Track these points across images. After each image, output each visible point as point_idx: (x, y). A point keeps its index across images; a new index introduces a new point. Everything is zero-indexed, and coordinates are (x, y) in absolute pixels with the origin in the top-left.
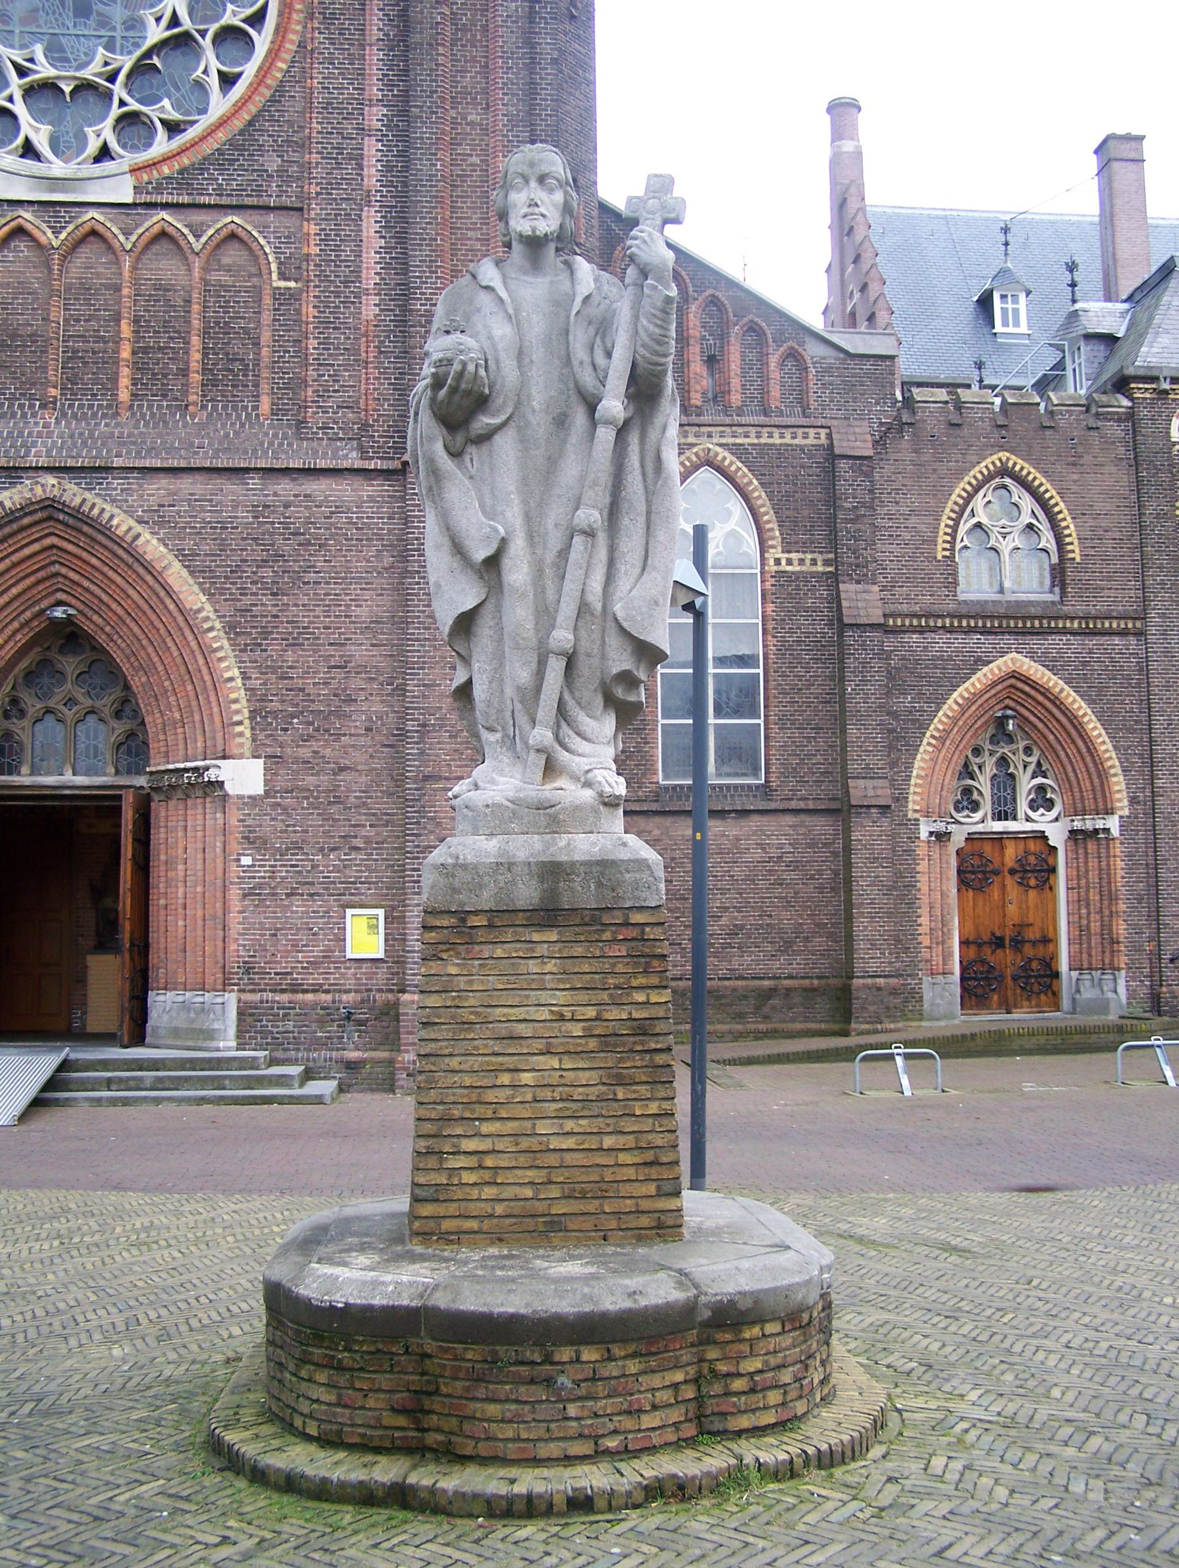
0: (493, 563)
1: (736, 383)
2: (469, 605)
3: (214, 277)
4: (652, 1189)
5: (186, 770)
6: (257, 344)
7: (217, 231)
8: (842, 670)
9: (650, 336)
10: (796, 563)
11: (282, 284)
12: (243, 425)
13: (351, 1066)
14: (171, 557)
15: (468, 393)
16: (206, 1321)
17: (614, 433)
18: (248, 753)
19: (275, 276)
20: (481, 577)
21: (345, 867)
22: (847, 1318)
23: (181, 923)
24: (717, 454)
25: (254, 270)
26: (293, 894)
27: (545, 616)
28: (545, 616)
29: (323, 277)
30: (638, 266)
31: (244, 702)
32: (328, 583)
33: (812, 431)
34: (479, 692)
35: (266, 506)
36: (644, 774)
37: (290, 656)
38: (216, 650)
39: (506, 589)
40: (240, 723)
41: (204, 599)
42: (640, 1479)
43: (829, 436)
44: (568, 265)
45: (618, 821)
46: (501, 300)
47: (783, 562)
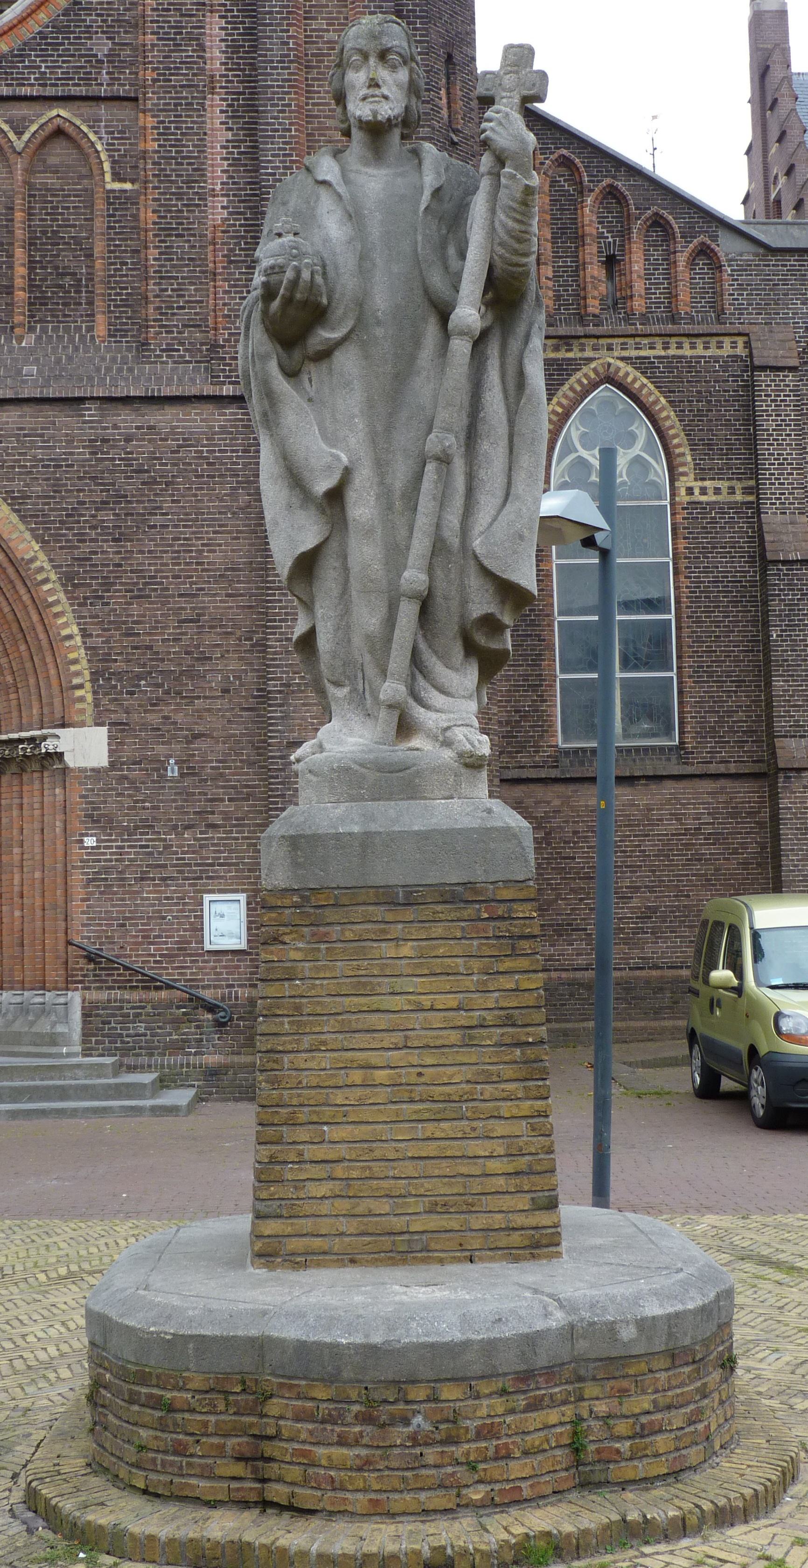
0: (336, 497)
1: (639, 287)
2: (309, 542)
3: (39, 180)
5: (21, 741)
6: (90, 256)
7: (41, 127)
8: (766, 613)
9: (509, 232)
10: (711, 492)
11: (117, 186)
12: (76, 349)
13: (213, 1073)
15: (305, 303)
17: (469, 346)
18: (89, 720)
19: (108, 177)
20: (323, 512)
21: (201, 846)
23: (17, 913)
25: (84, 171)
26: (142, 879)
27: (396, 556)
29: (162, 177)
31: (84, 663)
32: (176, 526)
33: (727, 341)
34: (324, 642)
35: (105, 441)
37: (135, 609)
38: (52, 605)
39: (351, 526)
40: (81, 686)
41: (37, 547)
43: (748, 345)
44: (416, 153)
45: (482, 788)
47: (697, 491)
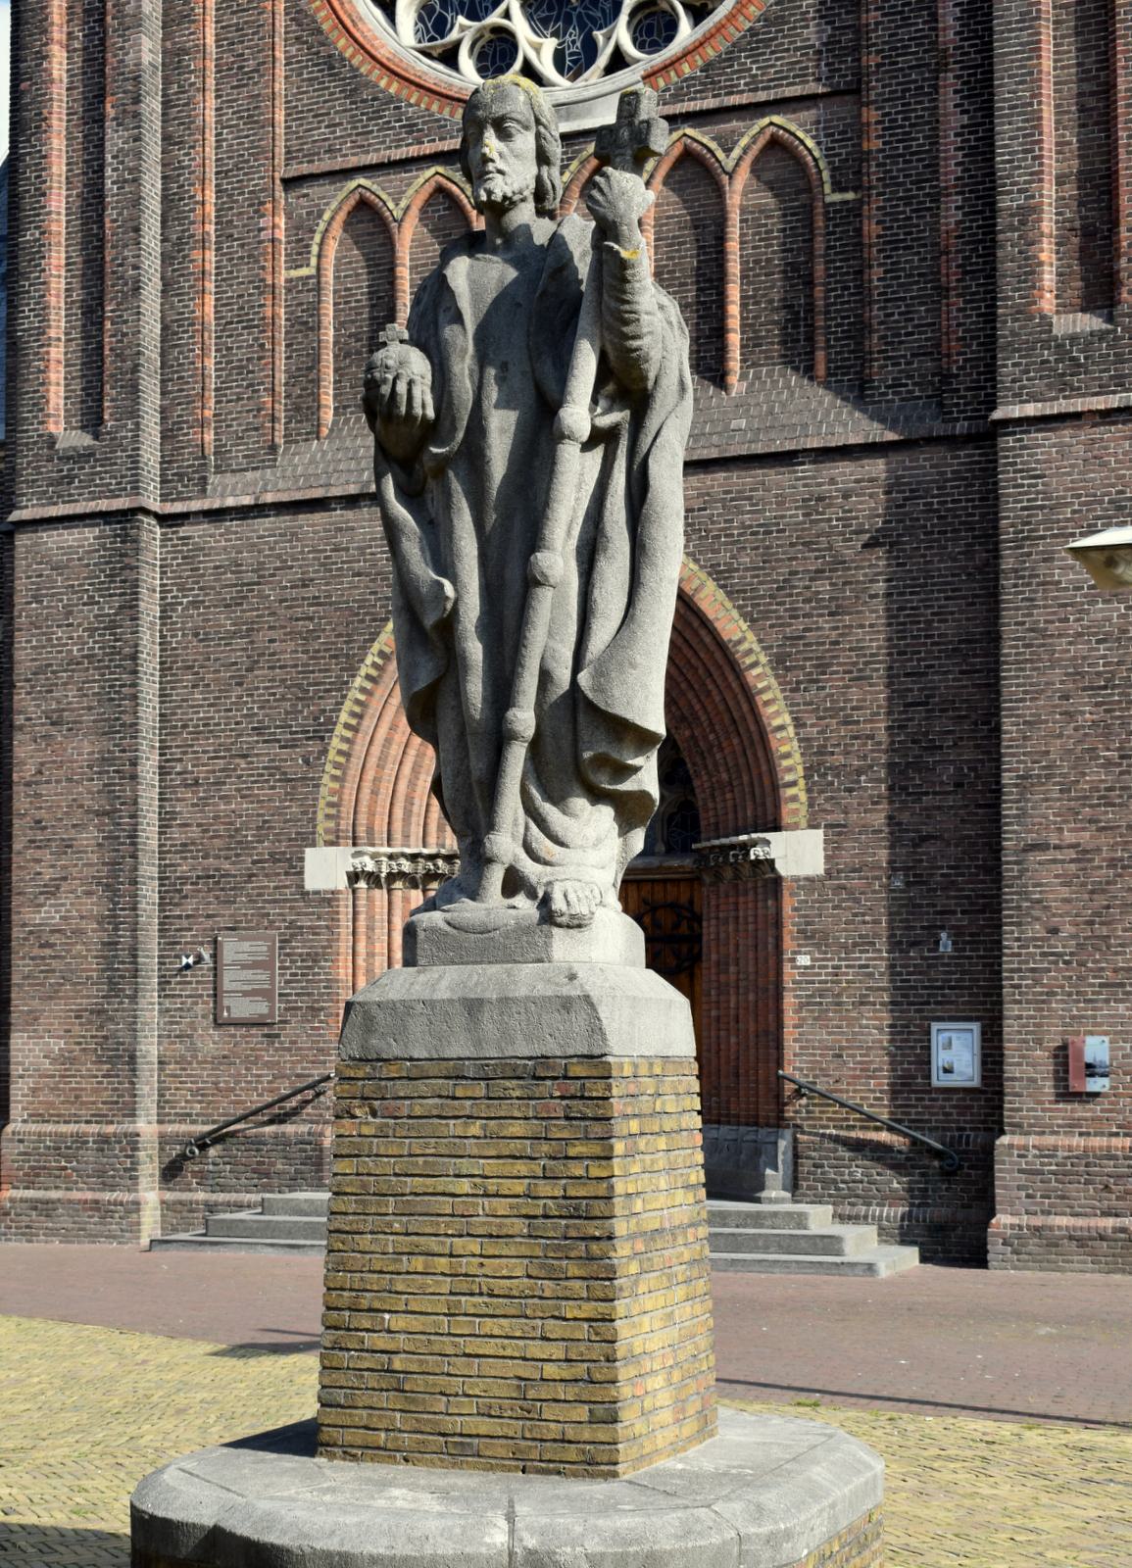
4: (582, 1413)
11: (837, 197)
14: (703, 575)
18: (804, 823)
19: (827, 188)
21: (929, 966)
26: (862, 1004)
31: (797, 757)
35: (820, 499)
37: (855, 694)
40: (794, 784)
41: (744, 626)
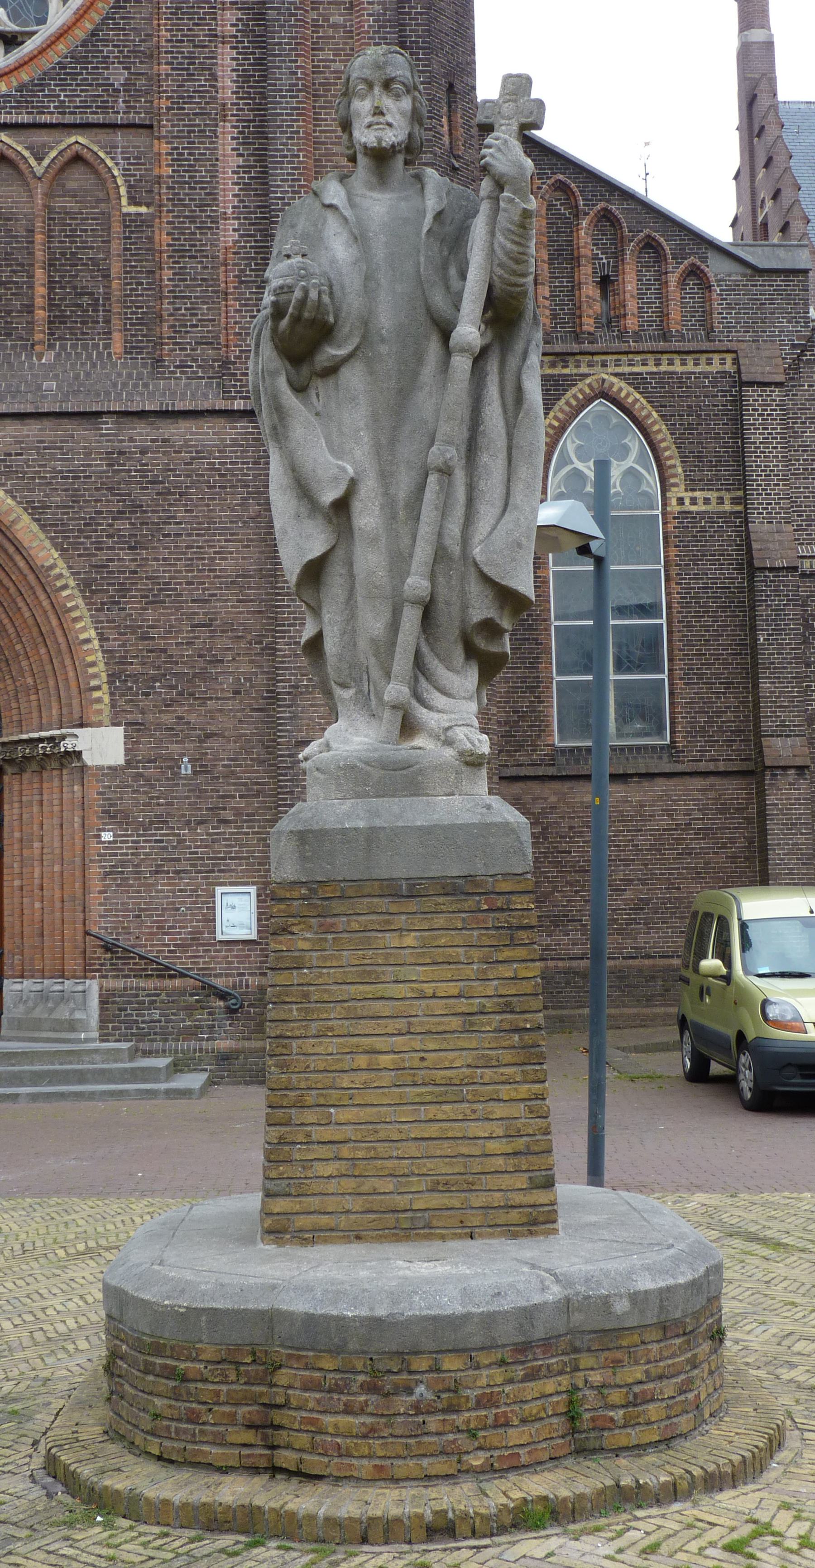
1: (632, 306)
2: (316, 550)
5: (41, 740)
6: (107, 276)
8: (753, 618)
9: (507, 253)
11: (133, 209)
12: (94, 365)
13: (224, 1058)
14: (20, 511)
15: (313, 322)
16: (52, 1335)
17: (469, 362)
18: (106, 721)
19: (124, 201)
20: (330, 521)
21: (213, 841)
22: (748, 1328)
23: (38, 905)
24: (612, 385)
25: (101, 195)
26: (157, 872)
27: (399, 563)
28: (399, 563)
30: (493, 177)
31: (102, 666)
32: (189, 535)
33: (716, 357)
34: (330, 646)
35: (121, 453)
36: (539, 736)
37: (150, 614)
40: (98, 688)
42: (504, 1500)
43: (736, 361)
44: (419, 178)
45: (482, 785)
46: (345, 219)
47: (687, 502)
